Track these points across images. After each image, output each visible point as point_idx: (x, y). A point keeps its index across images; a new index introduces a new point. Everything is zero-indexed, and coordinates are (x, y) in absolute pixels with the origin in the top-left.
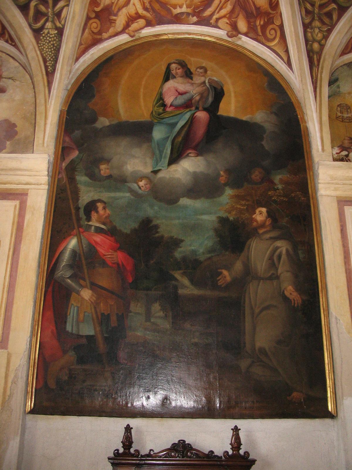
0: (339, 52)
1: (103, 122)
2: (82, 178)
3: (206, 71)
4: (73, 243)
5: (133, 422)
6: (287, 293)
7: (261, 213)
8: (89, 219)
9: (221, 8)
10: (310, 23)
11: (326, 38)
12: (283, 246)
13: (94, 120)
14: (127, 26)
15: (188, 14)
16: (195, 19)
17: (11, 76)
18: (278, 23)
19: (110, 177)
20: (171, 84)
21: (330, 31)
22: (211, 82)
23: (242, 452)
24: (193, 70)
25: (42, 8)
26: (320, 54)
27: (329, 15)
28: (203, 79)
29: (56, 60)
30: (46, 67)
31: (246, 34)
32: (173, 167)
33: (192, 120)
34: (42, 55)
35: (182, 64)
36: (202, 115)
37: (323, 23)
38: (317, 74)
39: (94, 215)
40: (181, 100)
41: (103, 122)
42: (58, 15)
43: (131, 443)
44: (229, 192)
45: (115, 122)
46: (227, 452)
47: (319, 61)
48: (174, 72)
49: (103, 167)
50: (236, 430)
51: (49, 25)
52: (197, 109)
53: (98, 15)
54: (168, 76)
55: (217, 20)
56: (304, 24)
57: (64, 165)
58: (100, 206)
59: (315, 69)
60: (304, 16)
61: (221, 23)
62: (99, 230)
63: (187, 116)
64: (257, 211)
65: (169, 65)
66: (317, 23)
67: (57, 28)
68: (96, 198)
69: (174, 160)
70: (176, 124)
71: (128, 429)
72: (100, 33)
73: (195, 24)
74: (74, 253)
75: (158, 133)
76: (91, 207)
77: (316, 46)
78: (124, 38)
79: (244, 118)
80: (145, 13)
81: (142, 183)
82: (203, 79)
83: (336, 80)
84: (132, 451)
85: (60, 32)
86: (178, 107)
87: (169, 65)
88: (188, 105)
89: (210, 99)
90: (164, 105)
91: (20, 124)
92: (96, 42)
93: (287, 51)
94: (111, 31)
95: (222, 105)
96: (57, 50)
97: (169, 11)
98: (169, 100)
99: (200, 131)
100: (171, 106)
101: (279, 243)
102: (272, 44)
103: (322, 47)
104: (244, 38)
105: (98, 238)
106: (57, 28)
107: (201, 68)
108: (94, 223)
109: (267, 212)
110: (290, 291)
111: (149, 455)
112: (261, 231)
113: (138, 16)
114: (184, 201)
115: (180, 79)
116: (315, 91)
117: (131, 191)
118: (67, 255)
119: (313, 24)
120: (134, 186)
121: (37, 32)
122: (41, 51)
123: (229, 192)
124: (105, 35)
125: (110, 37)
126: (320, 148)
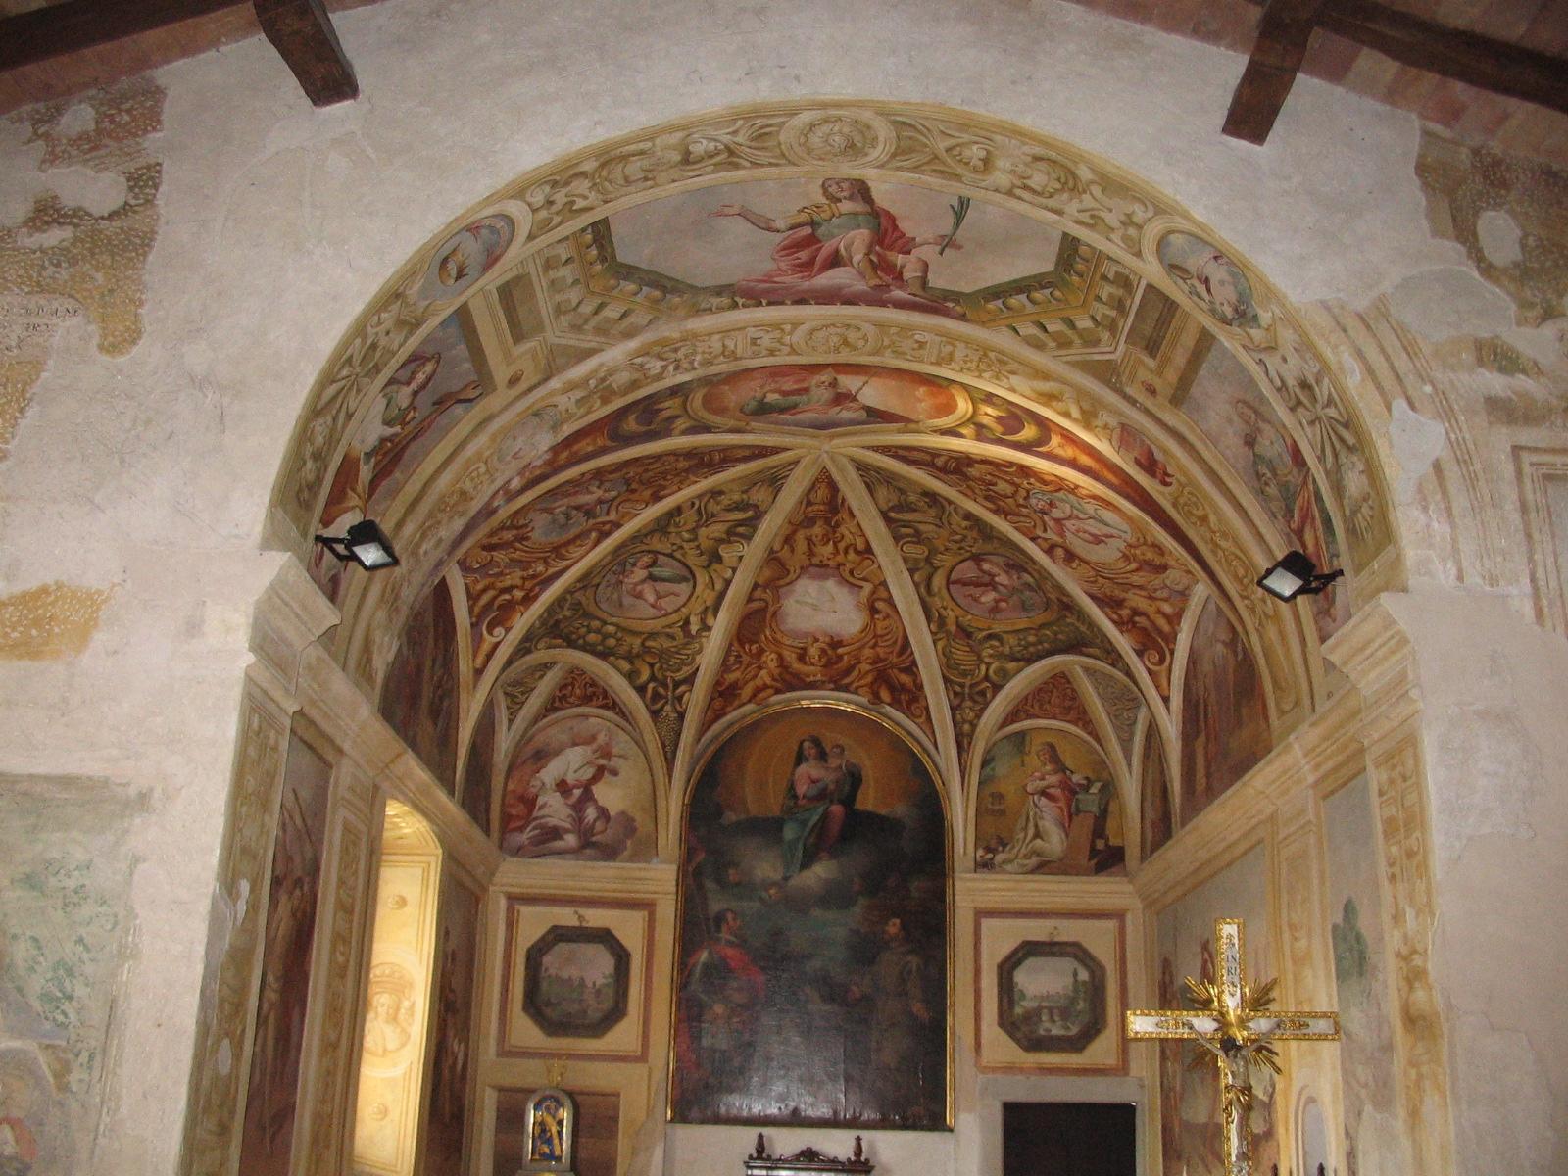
0: (995, 728)
1: (731, 817)
2: (710, 885)
3: (843, 750)
4: (704, 956)
5: (767, 1131)
6: (915, 1010)
7: (894, 925)
8: (719, 930)
9: (861, 679)
10: (959, 705)
11: (978, 717)
12: (914, 961)
13: (720, 814)
14: (754, 695)
15: (823, 682)
16: (832, 686)
17: (622, 752)
18: (924, 703)
19: (738, 884)
20: (803, 768)
21: (982, 710)
22: (849, 765)
23: (863, 1159)
24: (828, 750)
25: (661, 690)
26: (971, 735)
27: (983, 693)
28: (838, 762)
29: (676, 745)
30: (665, 753)
31: (889, 704)
32: (806, 874)
33: (826, 816)
34: (661, 739)
35: (817, 742)
36: (837, 809)
37: (975, 702)
38: (1085, 460)
39: (724, 928)
40: (814, 791)
41: (731, 817)
42: (680, 698)
43: (763, 1149)
44: (862, 901)
45: (743, 817)
46: (849, 1159)
47: (970, 743)
48: (806, 753)
49: (731, 872)
50: (859, 1139)
51: (668, 707)
52: (832, 802)
53: (721, 694)
54: (800, 759)
55: (857, 688)
56: (952, 708)
57: (690, 869)
58: (730, 916)
59: (965, 755)
60: (952, 697)
61: (860, 691)
62: (731, 944)
63: (821, 810)
64: (890, 923)
65: (801, 743)
66: (968, 703)
67: (678, 712)
68: (726, 906)
69: (806, 864)
70: (808, 820)
71: (761, 1137)
72: (723, 709)
73: (832, 690)
74: (706, 966)
75: (789, 832)
76: (720, 919)
77: (967, 727)
78: (750, 707)
79: (883, 812)
80: (774, 683)
81: (772, 891)
82: (838, 762)
83: (992, 759)
84: (764, 1156)
85: (681, 716)
86: (811, 799)
87: (801, 743)
88: (823, 795)
89: (847, 788)
90: (795, 796)
91: (638, 817)
92: (718, 718)
93: (933, 732)
94: (736, 703)
95: (860, 796)
96: (679, 735)
97: (803, 681)
98: (802, 789)
99: (835, 829)
100: (804, 797)
101: (909, 958)
102: (917, 721)
103: (974, 726)
104: (888, 708)
105: (730, 952)
106: (678, 712)
107: (838, 746)
108: (724, 935)
109: (901, 923)
110: (918, 1008)
111: (780, 1160)
112: (893, 945)
113: (766, 687)
114: (817, 913)
115: (813, 762)
116: (963, 785)
117: (761, 899)
118: (699, 968)
119: (964, 705)
120: (764, 894)
121: (655, 714)
122: (659, 734)
123: (862, 901)
124: (729, 709)
125: (735, 709)
126: (962, 850)
